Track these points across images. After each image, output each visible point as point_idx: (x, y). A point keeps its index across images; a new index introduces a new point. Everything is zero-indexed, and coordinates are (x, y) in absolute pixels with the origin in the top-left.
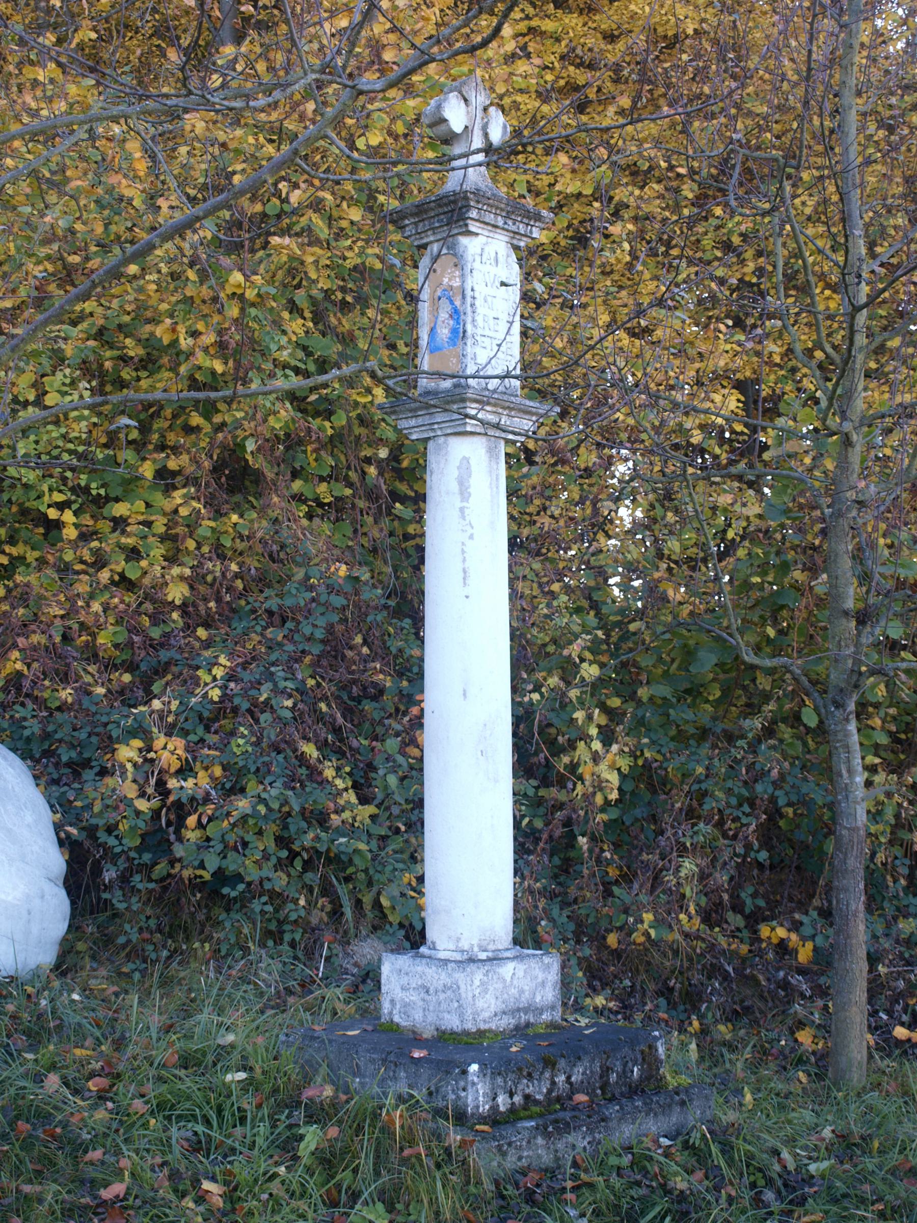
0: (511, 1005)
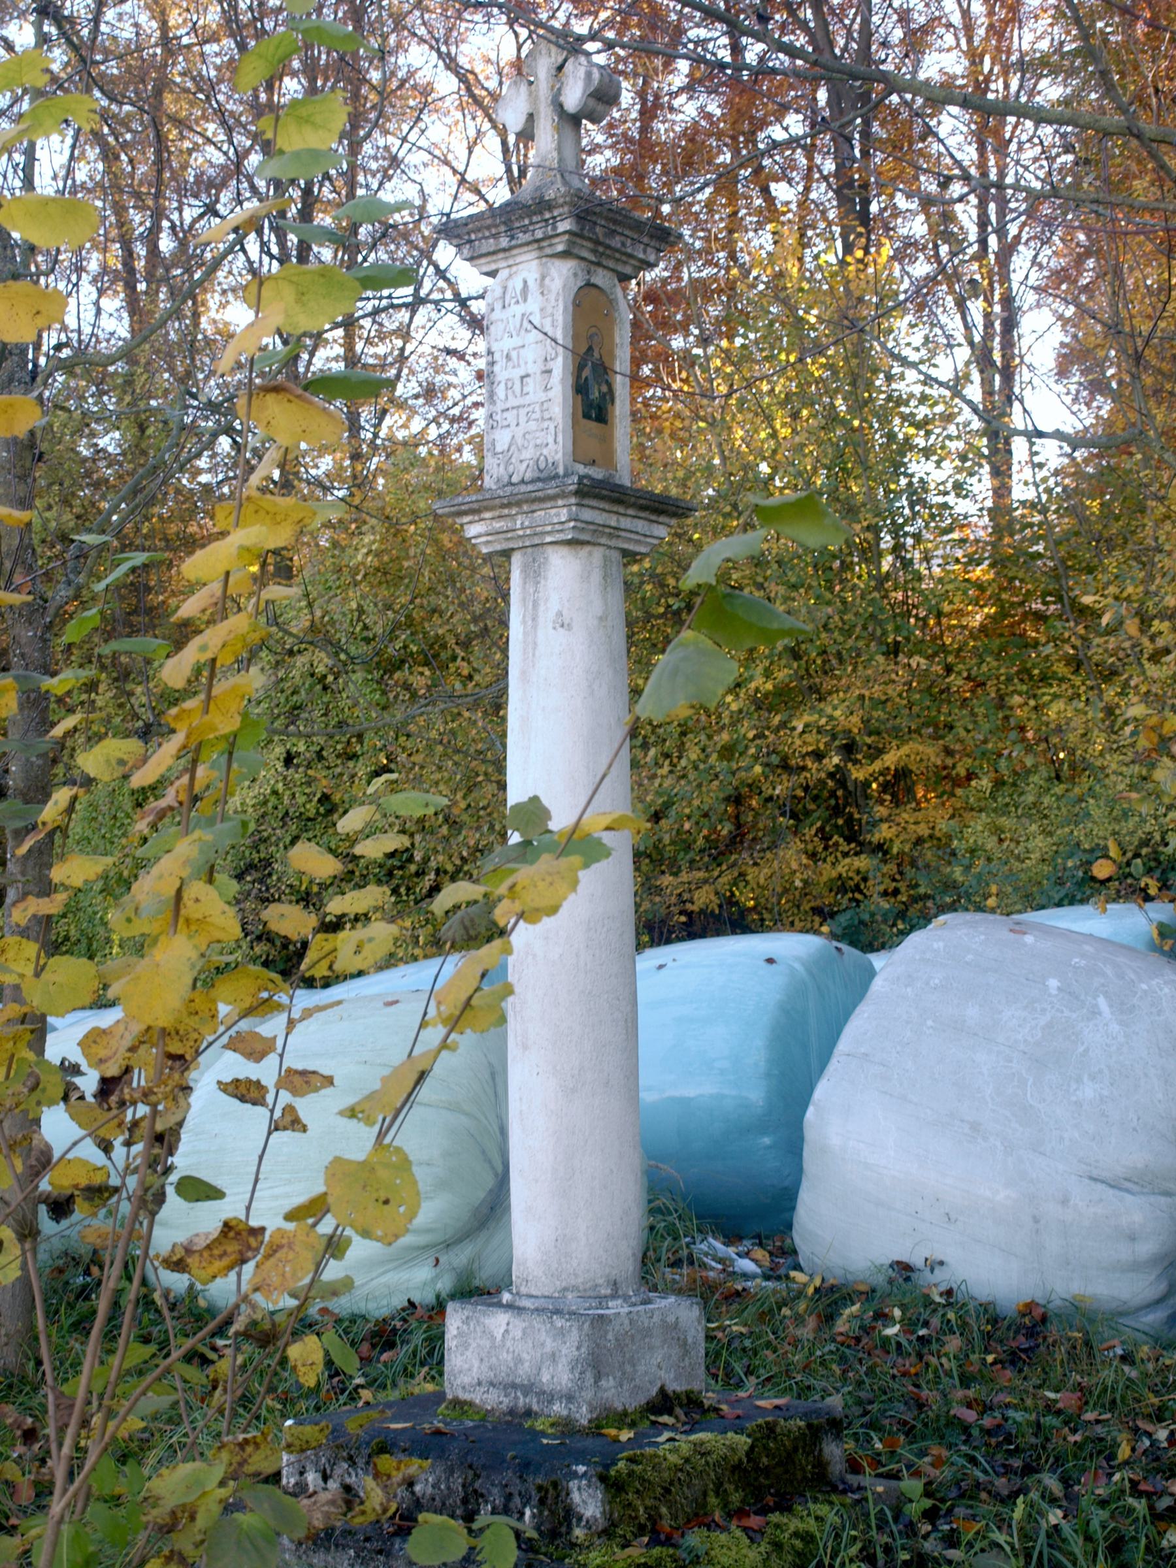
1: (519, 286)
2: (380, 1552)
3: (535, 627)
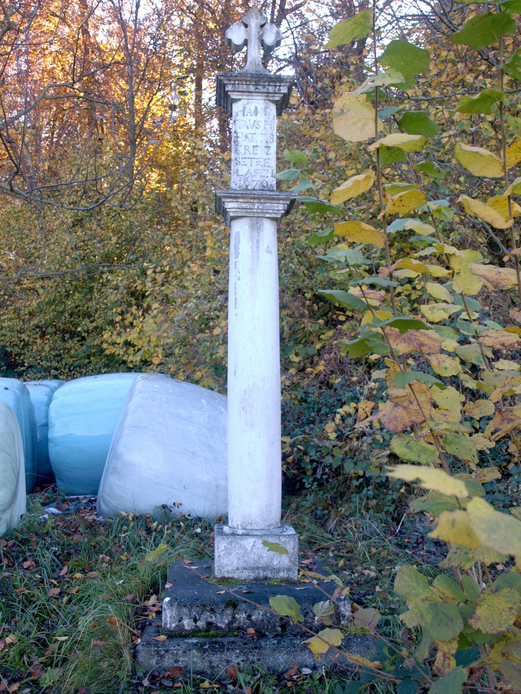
0: (251, 564)
1: (253, 109)
2: (256, 648)
3: (258, 251)
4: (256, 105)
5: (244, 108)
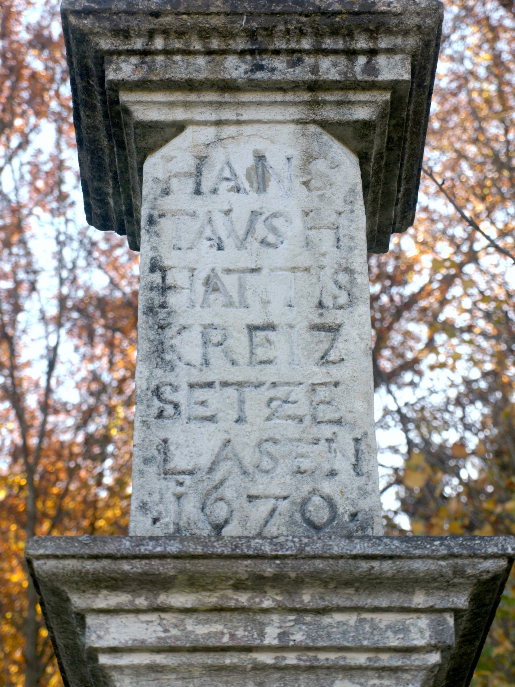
1: (243, 162)
4: (261, 145)
5: (202, 160)
